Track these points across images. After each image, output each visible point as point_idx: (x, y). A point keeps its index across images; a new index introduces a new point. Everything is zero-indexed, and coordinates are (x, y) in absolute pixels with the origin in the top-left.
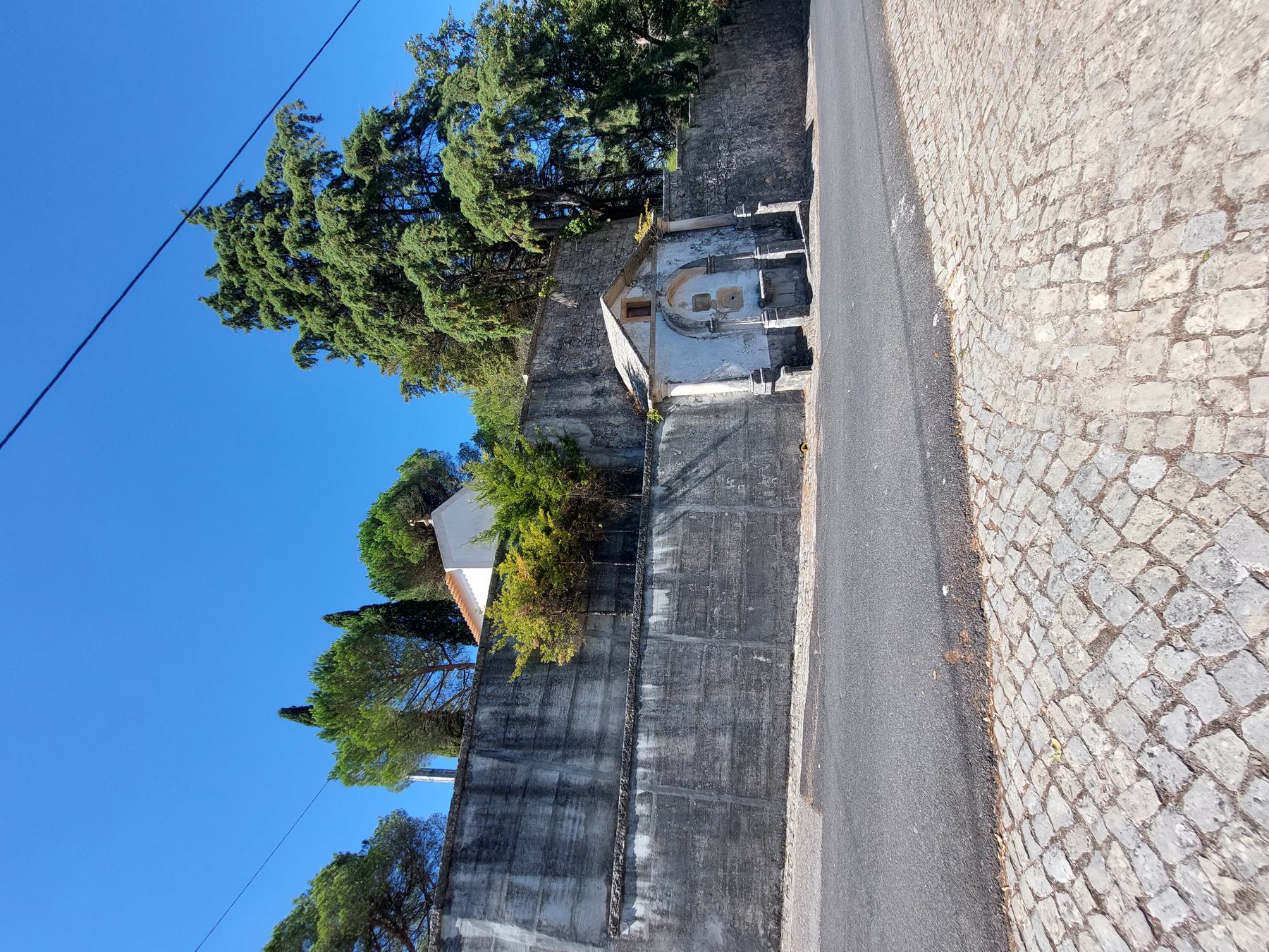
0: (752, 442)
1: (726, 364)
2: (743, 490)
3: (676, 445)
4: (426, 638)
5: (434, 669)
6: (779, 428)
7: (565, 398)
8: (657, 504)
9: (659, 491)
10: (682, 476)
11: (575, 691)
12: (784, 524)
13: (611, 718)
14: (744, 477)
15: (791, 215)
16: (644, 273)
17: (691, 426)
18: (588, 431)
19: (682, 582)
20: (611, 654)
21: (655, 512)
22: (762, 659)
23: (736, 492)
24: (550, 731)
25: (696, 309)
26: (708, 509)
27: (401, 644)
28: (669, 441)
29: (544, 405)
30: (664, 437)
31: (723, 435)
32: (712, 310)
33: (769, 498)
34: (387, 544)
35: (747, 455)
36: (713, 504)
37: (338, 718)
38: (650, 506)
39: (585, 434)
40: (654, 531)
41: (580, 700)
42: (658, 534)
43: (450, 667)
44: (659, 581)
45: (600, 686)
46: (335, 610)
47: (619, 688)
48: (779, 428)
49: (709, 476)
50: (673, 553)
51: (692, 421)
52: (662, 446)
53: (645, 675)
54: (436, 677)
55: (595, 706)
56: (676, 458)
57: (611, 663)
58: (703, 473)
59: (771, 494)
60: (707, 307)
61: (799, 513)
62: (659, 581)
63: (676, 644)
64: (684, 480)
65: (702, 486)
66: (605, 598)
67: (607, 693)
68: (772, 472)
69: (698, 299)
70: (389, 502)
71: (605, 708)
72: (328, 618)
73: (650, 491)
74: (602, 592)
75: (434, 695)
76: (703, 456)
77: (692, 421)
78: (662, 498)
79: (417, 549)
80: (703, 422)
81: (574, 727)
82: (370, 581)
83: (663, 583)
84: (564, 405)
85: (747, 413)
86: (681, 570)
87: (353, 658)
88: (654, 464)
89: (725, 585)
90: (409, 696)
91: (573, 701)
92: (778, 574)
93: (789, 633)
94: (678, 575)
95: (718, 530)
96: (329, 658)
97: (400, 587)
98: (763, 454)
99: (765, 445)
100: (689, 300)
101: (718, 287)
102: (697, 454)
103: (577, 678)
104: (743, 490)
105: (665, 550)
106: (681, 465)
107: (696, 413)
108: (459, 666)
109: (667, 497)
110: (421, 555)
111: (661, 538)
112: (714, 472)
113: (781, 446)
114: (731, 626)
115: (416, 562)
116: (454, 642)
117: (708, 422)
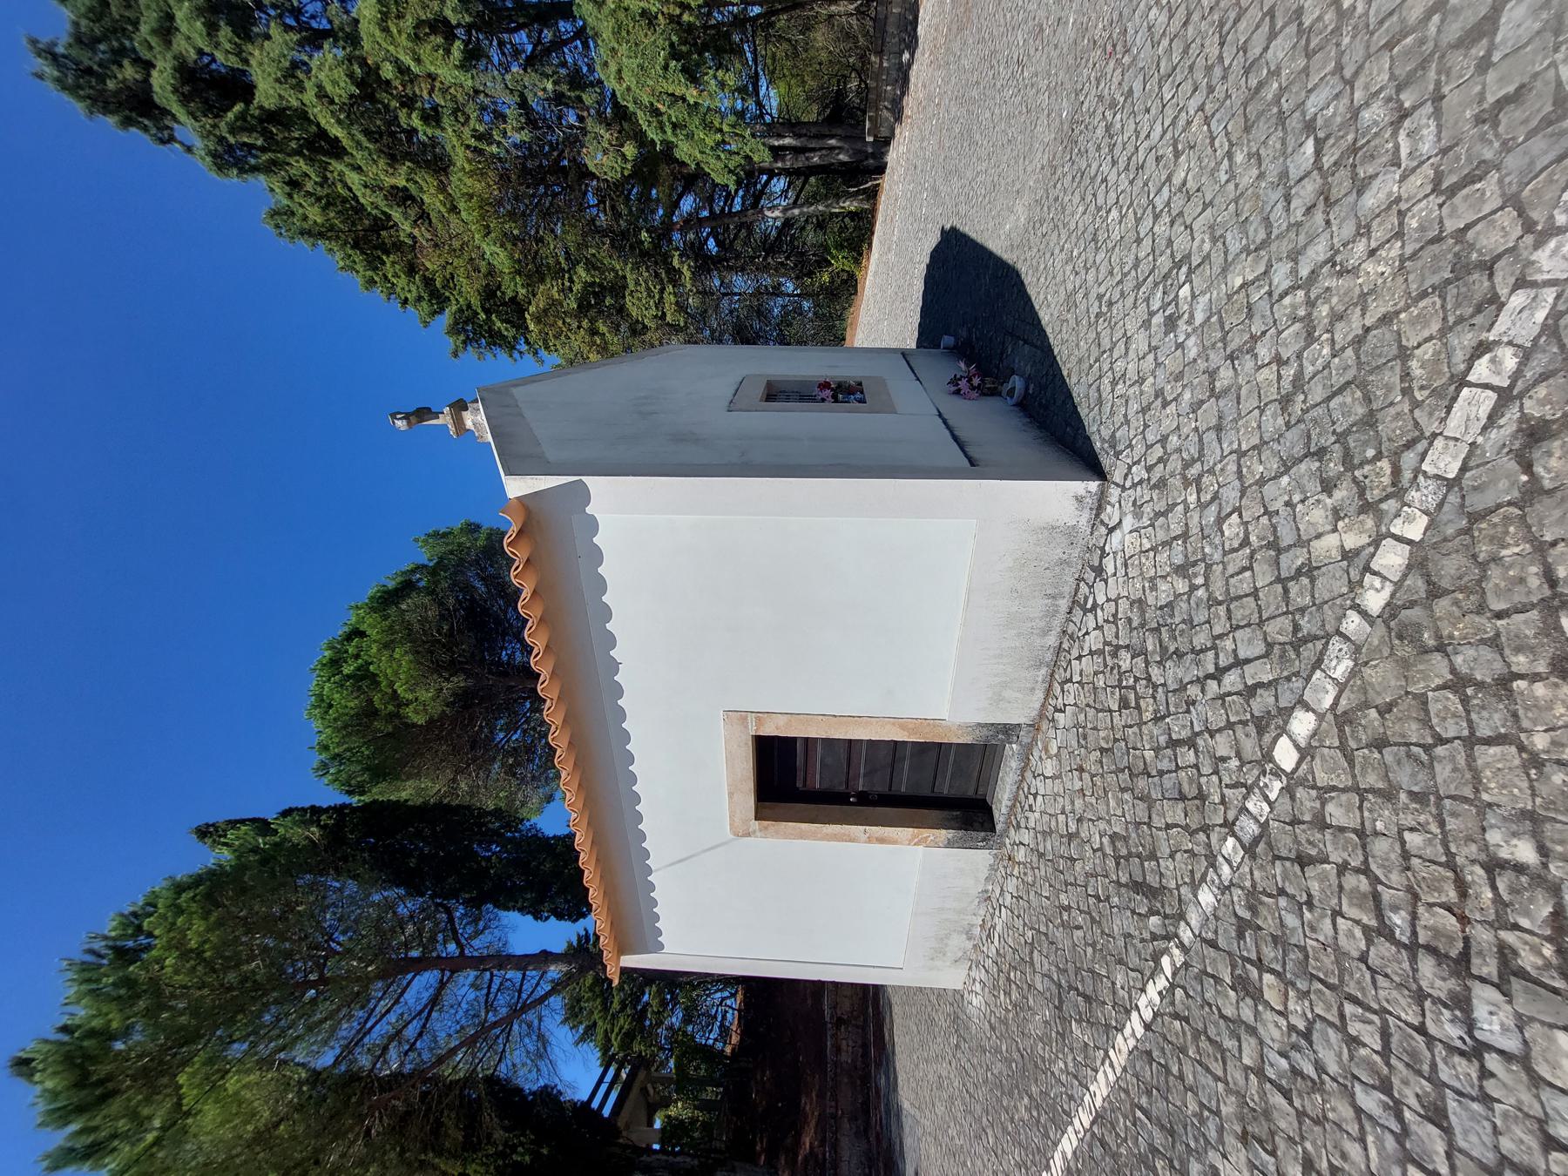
4: (415, 890)
5: (419, 965)
27: (356, 901)
34: (365, 678)
37: (116, 1106)
43: (455, 965)
46: (219, 816)
54: (422, 984)
70: (387, 600)
75: (411, 1032)
79: (425, 695)
82: (318, 758)
87: (199, 925)
90: (347, 1029)
96: (134, 923)
97: (379, 773)
108: (478, 962)
110: (436, 709)
115: (420, 720)
116: (475, 903)
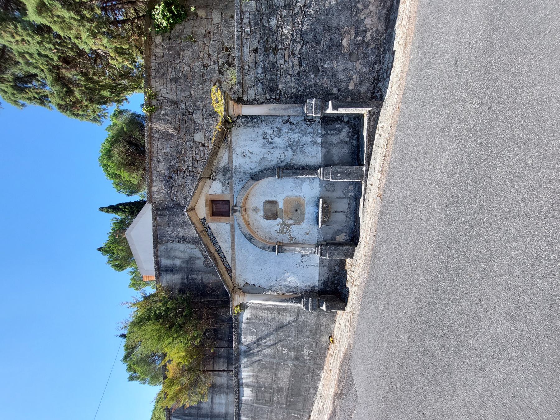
0: (300, 331)
1: (287, 275)
2: (292, 354)
3: (252, 325)
6: (318, 326)
7: (181, 226)
8: (243, 354)
9: (243, 348)
10: (257, 343)
11: (212, 398)
12: (313, 372)
13: (230, 408)
14: (294, 348)
15: (360, 117)
16: (222, 165)
17: (262, 317)
18: (201, 256)
19: (258, 387)
20: (227, 384)
21: (242, 357)
22: (296, 415)
23: (288, 354)
24: (203, 412)
25: (267, 217)
26: (272, 360)
28: (248, 323)
29: (169, 232)
30: (244, 320)
31: (282, 324)
32: (279, 220)
33: (307, 360)
35: (296, 337)
36: (275, 358)
38: (239, 354)
39: (199, 258)
40: (242, 366)
41: (215, 401)
42: (244, 367)
44: (246, 385)
45: (224, 396)
47: (232, 397)
48: (318, 326)
49: (273, 345)
50: (253, 376)
51: (261, 314)
52: (243, 326)
53: (242, 415)
55: (222, 404)
56: (252, 333)
57: (228, 387)
58: (268, 343)
59: (308, 358)
60: (274, 216)
61: (323, 368)
62: (246, 385)
63: (256, 407)
64: (258, 345)
65: (269, 350)
66: (222, 360)
67: (227, 399)
68: (310, 348)
69: (269, 206)
71: (227, 405)
72: (102, 209)
73: (238, 348)
74: (220, 357)
76: (269, 334)
77: (261, 314)
78: (245, 352)
80: (269, 315)
81: (214, 411)
83: (248, 386)
84: (181, 232)
85: (298, 315)
86: (257, 383)
88: (239, 335)
89: (280, 390)
91: (212, 402)
92: (308, 390)
93: (310, 409)
94: (256, 384)
95: (277, 370)
98: (307, 338)
99: (308, 334)
100: (261, 206)
101: (286, 194)
102: (266, 333)
103: (213, 393)
104: (292, 354)
105: (249, 374)
106: (256, 338)
107: (264, 309)
109: (248, 352)
111: (246, 369)
112: (276, 344)
113: (318, 336)
114: (283, 404)
117: (273, 316)
